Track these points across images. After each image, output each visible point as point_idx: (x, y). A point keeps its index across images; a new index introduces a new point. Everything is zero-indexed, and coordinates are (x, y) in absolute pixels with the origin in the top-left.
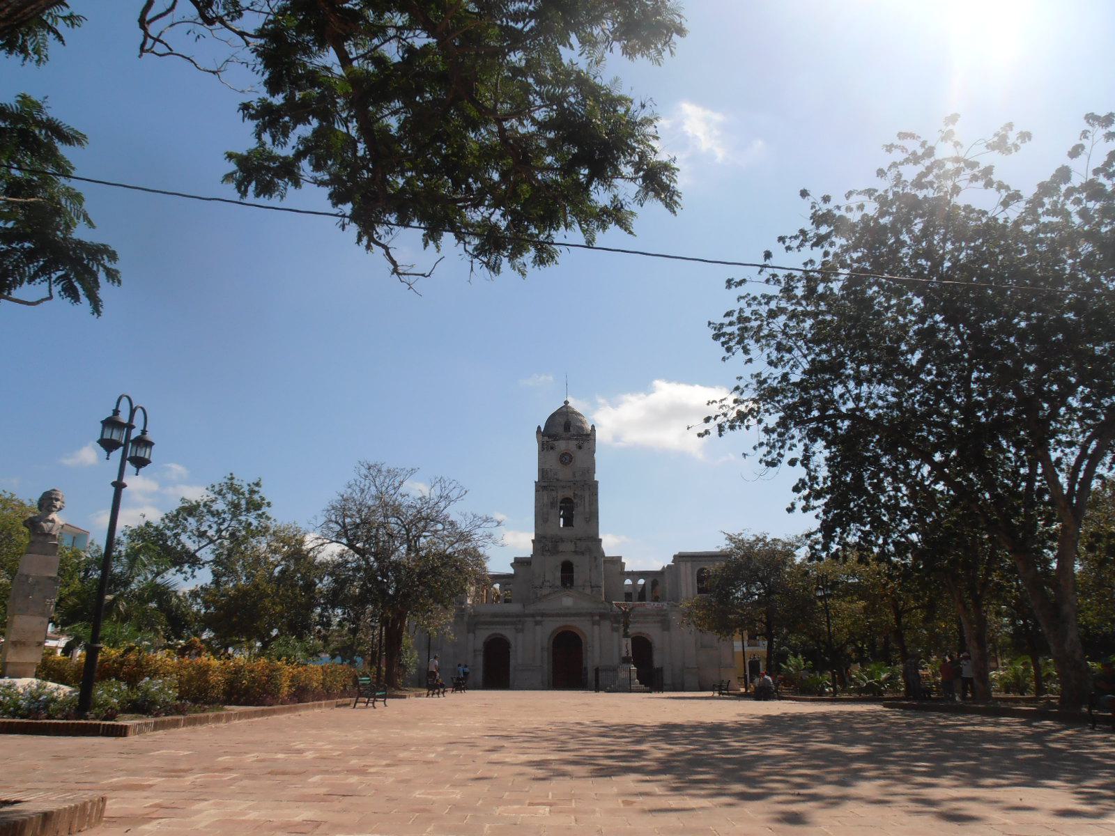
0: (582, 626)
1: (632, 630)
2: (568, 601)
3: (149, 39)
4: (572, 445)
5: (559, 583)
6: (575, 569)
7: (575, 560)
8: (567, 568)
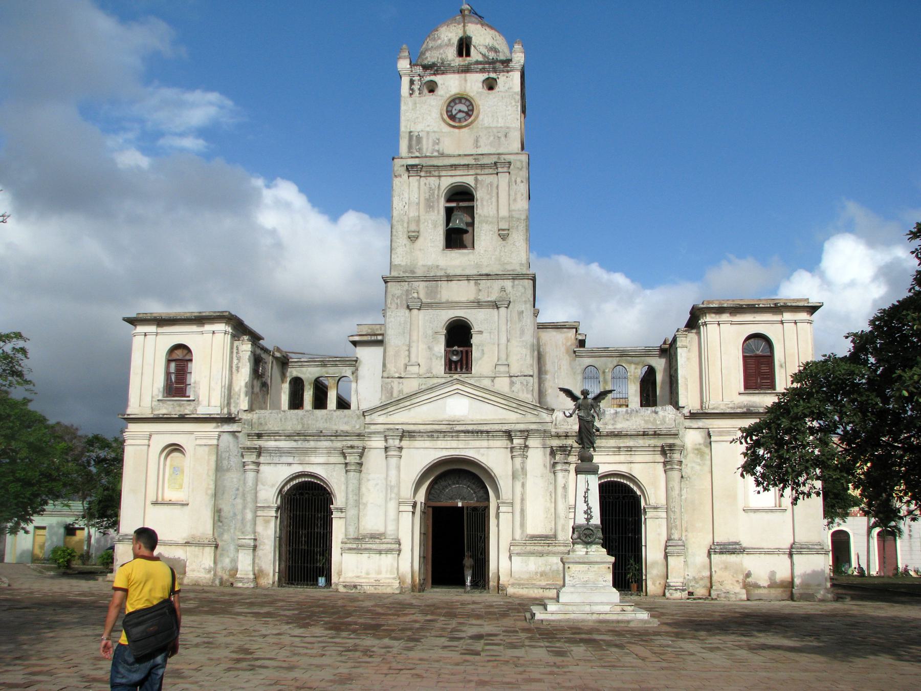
0: (492, 456)
1: (607, 461)
2: (458, 406)
3: (555, 591)
4: (473, 83)
5: (439, 367)
6: (475, 340)
7: (477, 318)
8: (459, 335)
